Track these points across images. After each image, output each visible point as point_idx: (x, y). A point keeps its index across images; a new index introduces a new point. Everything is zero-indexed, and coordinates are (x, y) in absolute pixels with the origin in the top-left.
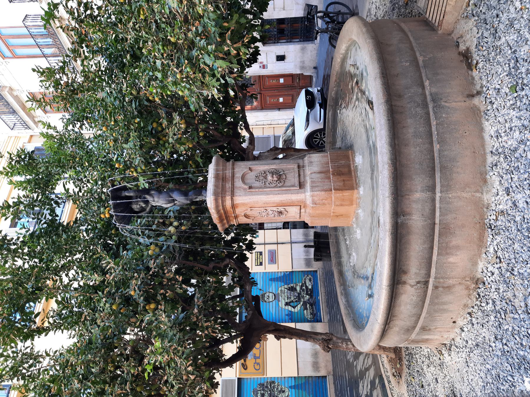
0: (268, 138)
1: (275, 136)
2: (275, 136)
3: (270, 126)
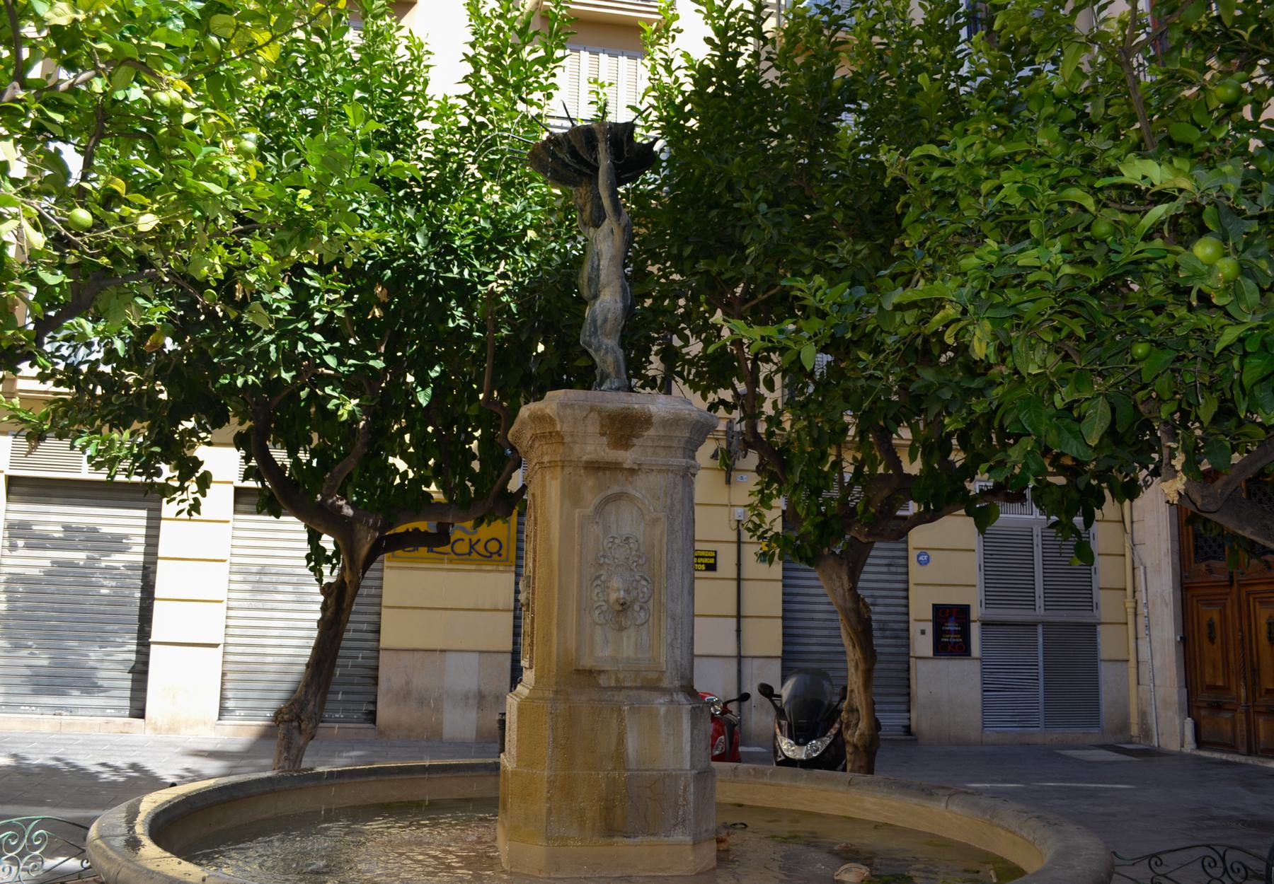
0: (1090, 605)
3: (1130, 611)
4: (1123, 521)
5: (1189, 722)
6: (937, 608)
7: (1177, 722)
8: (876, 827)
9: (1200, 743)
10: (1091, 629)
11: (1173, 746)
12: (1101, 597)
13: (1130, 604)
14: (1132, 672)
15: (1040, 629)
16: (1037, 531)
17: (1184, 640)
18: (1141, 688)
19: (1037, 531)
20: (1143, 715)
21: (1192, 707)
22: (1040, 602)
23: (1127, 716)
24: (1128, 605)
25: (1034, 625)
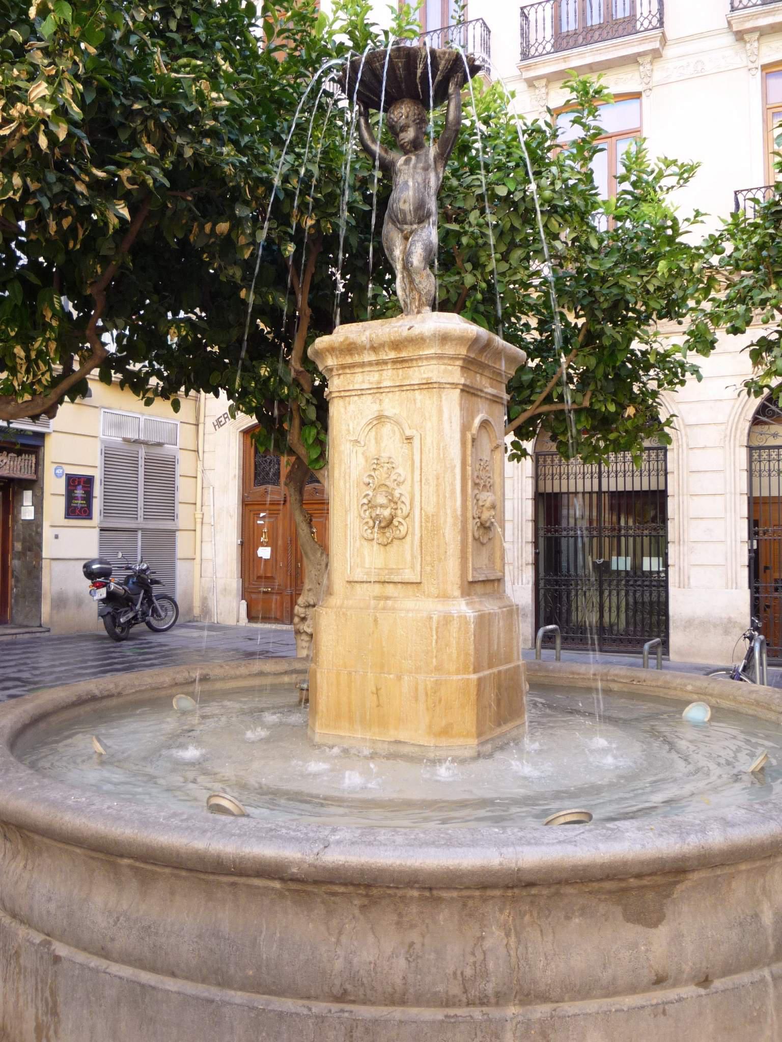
0: (173, 517)
1: (174, 531)
2: (174, 531)
3: (199, 520)
4: (198, 451)
5: (244, 604)
6: (91, 519)
7: (235, 604)
8: (485, 527)
9: (251, 617)
10: (171, 534)
11: (232, 622)
12: (181, 510)
13: (199, 516)
14: (197, 568)
15: (140, 533)
16: (522, 669)
17: (242, 544)
18: (203, 580)
19: (522, 669)
20: (204, 600)
21: (247, 593)
22: (141, 513)
23: (192, 602)
24: (197, 516)
25: (135, 531)
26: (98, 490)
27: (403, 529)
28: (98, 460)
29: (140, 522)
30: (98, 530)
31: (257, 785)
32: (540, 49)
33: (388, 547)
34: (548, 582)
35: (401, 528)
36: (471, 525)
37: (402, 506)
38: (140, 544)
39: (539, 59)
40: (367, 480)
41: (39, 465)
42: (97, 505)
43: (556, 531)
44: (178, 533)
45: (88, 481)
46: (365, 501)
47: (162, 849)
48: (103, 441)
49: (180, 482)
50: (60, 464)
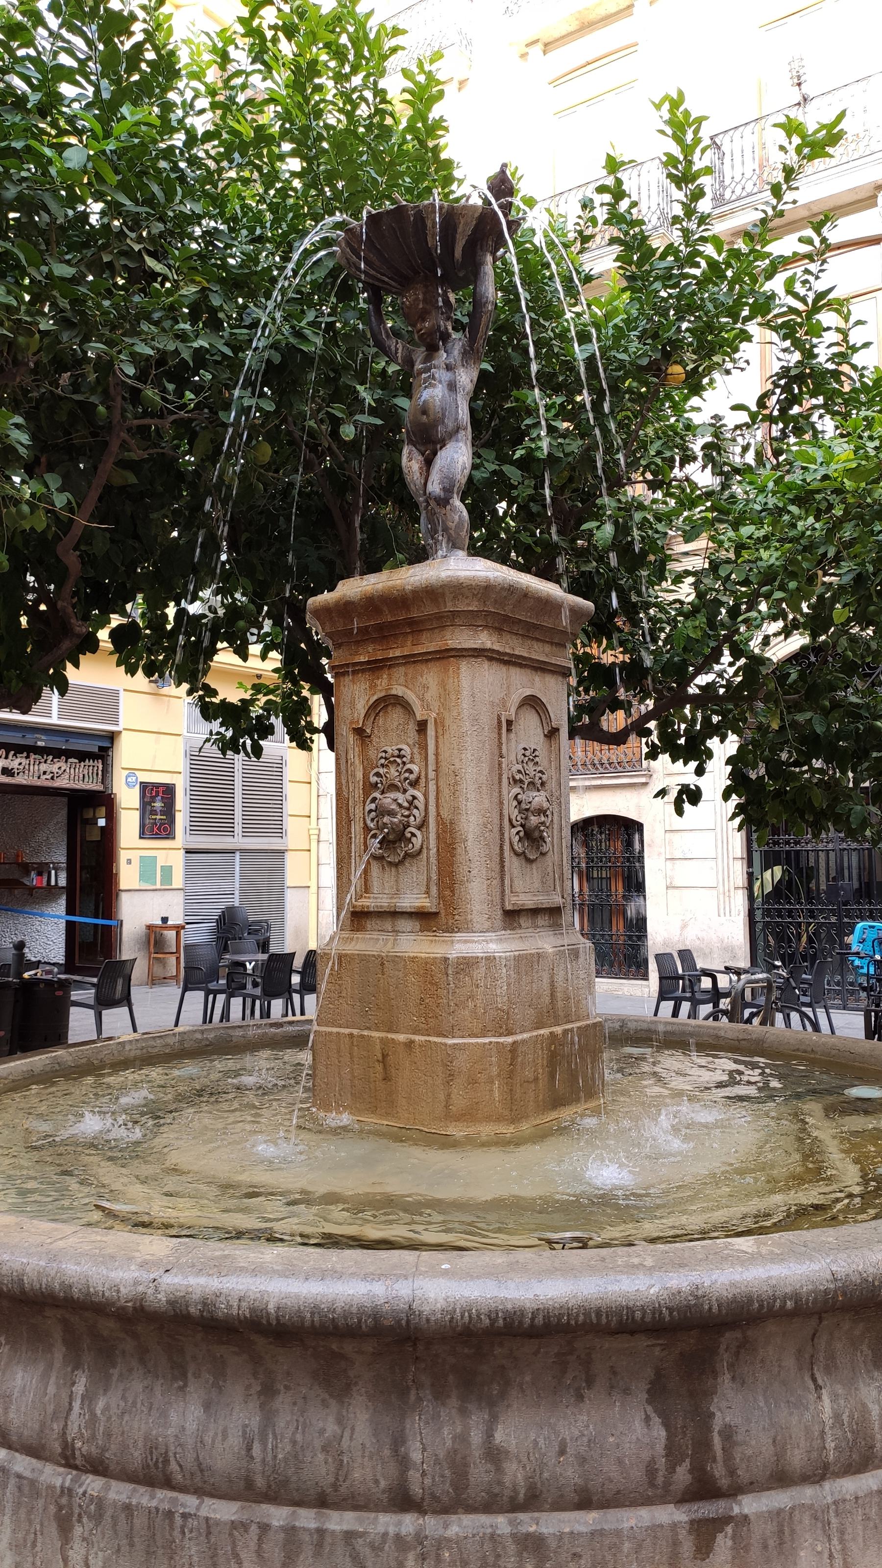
0: (280, 832)
1: (282, 852)
2: (282, 852)
12: (291, 825)
22: (238, 829)
25: (232, 852)
26: (181, 802)
27: (417, 842)
28: (180, 764)
29: (238, 841)
30: (182, 852)
31: (830, 1277)
32: (738, 191)
33: (401, 869)
34: (767, 912)
35: (414, 839)
36: (512, 835)
37: (415, 811)
38: (237, 868)
39: (737, 204)
40: (374, 779)
41: (106, 773)
42: (181, 820)
43: (797, 843)
44: (288, 856)
45: (168, 791)
46: (373, 806)
47: (315, 1309)
48: (185, 738)
49: (289, 789)
50: (132, 771)
